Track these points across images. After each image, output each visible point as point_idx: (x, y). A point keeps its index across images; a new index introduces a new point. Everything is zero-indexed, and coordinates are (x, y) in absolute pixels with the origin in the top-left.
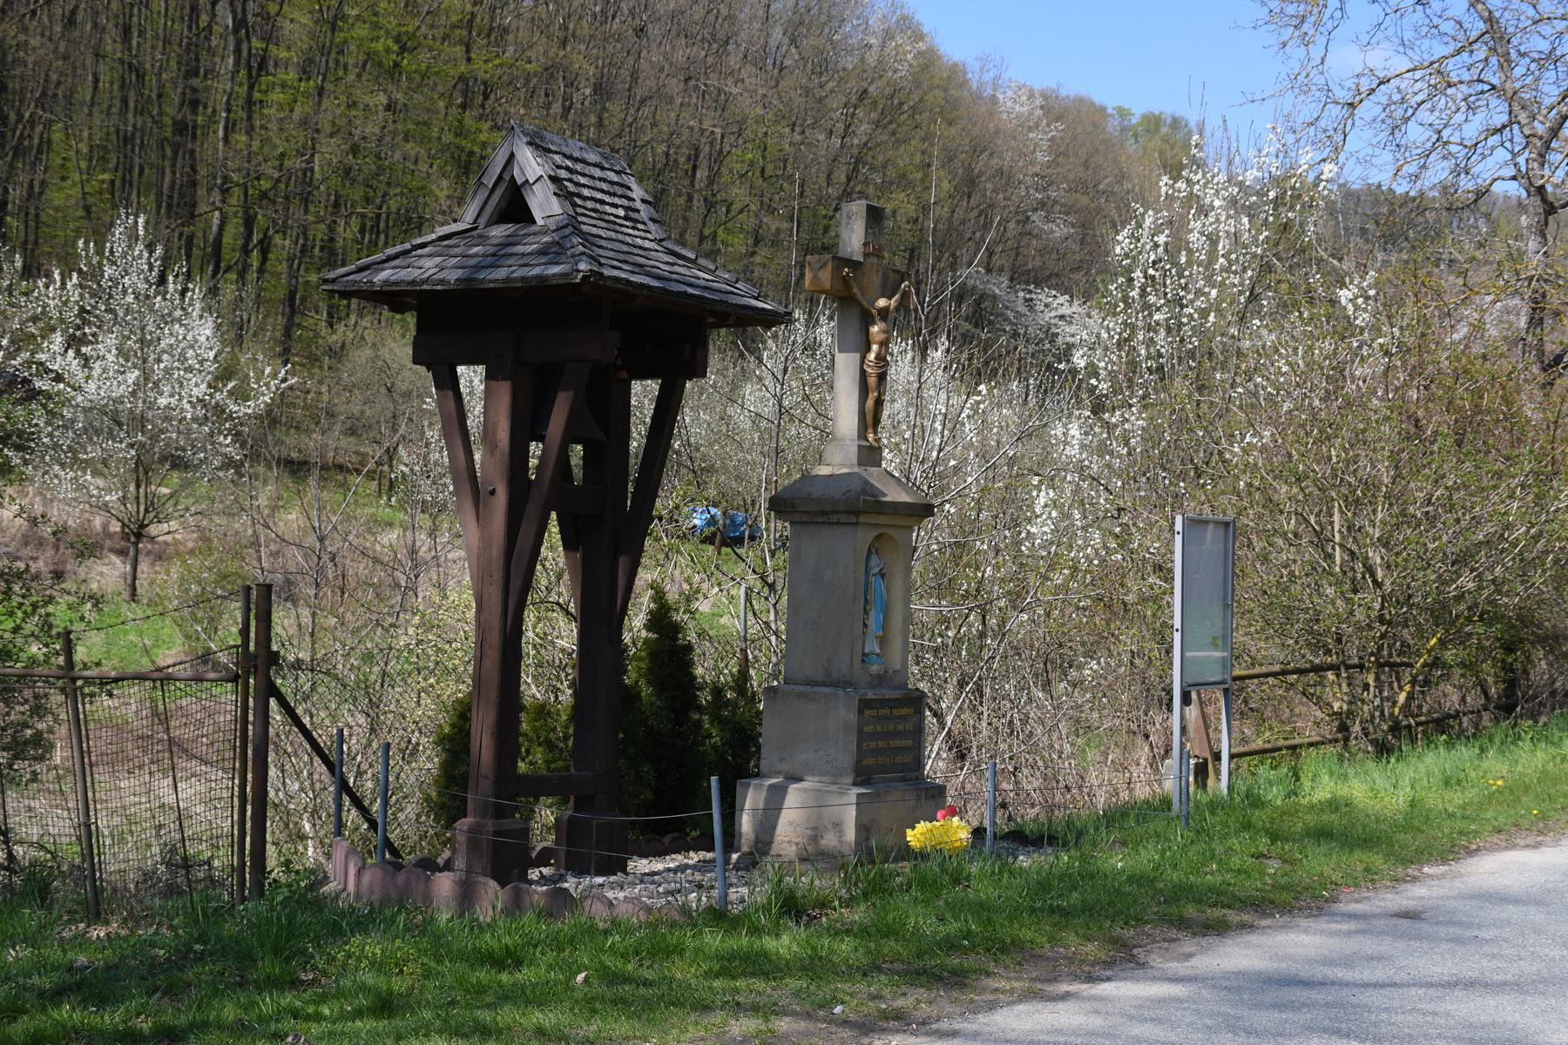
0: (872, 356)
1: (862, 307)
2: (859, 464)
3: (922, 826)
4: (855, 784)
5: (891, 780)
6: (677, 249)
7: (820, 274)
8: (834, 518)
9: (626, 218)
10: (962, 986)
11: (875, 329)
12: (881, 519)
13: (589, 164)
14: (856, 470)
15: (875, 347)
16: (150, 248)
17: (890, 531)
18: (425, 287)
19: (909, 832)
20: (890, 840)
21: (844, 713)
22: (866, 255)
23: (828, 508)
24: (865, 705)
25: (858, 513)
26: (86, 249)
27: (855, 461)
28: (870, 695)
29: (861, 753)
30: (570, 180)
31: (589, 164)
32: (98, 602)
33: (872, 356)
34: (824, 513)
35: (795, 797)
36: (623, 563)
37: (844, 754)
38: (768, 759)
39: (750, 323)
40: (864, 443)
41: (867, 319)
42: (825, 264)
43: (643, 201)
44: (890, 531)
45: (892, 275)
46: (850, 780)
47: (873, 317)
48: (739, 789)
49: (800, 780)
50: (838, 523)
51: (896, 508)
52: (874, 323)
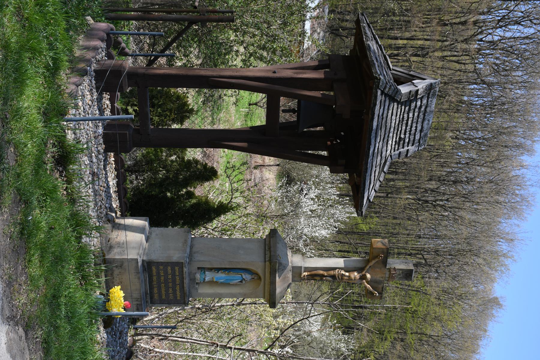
0: (343, 272)
1: (365, 267)
2: (293, 267)
3: (122, 294)
4: (143, 261)
5: (145, 285)
6: (388, 163)
7: (379, 243)
8: (268, 253)
9: (400, 138)
10: (16, 251)
11: (356, 274)
12: (267, 275)
13: (423, 123)
14: (290, 264)
15: (347, 274)
16: (348, 218)
17: (262, 283)
18: (364, 36)
19: (119, 287)
20: (117, 280)
21: (176, 256)
22: (389, 270)
23: (272, 249)
24: (180, 265)
25: (270, 261)
26: (346, 200)
27: (294, 265)
28: (185, 270)
29: (158, 264)
30: (416, 106)
31: (423, 123)
32: (235, 104)
33: (343, 272)
34: (270, 248)
35: (140, 237)
36: (244, 145)
37: (158, 256)
38: (157, 230)
39: (356, 193)
40: (303, 270)
41: (360, 270)
42: (385, 245)
43: (408, 150)
44: (262, 283)
45: (380, 286)
46: (145, 259)
47: (361, 272)
48: (145, 218)
49: (147, 241)
50: (265, 255)
51: (273, 283)
52: (358, 273)
